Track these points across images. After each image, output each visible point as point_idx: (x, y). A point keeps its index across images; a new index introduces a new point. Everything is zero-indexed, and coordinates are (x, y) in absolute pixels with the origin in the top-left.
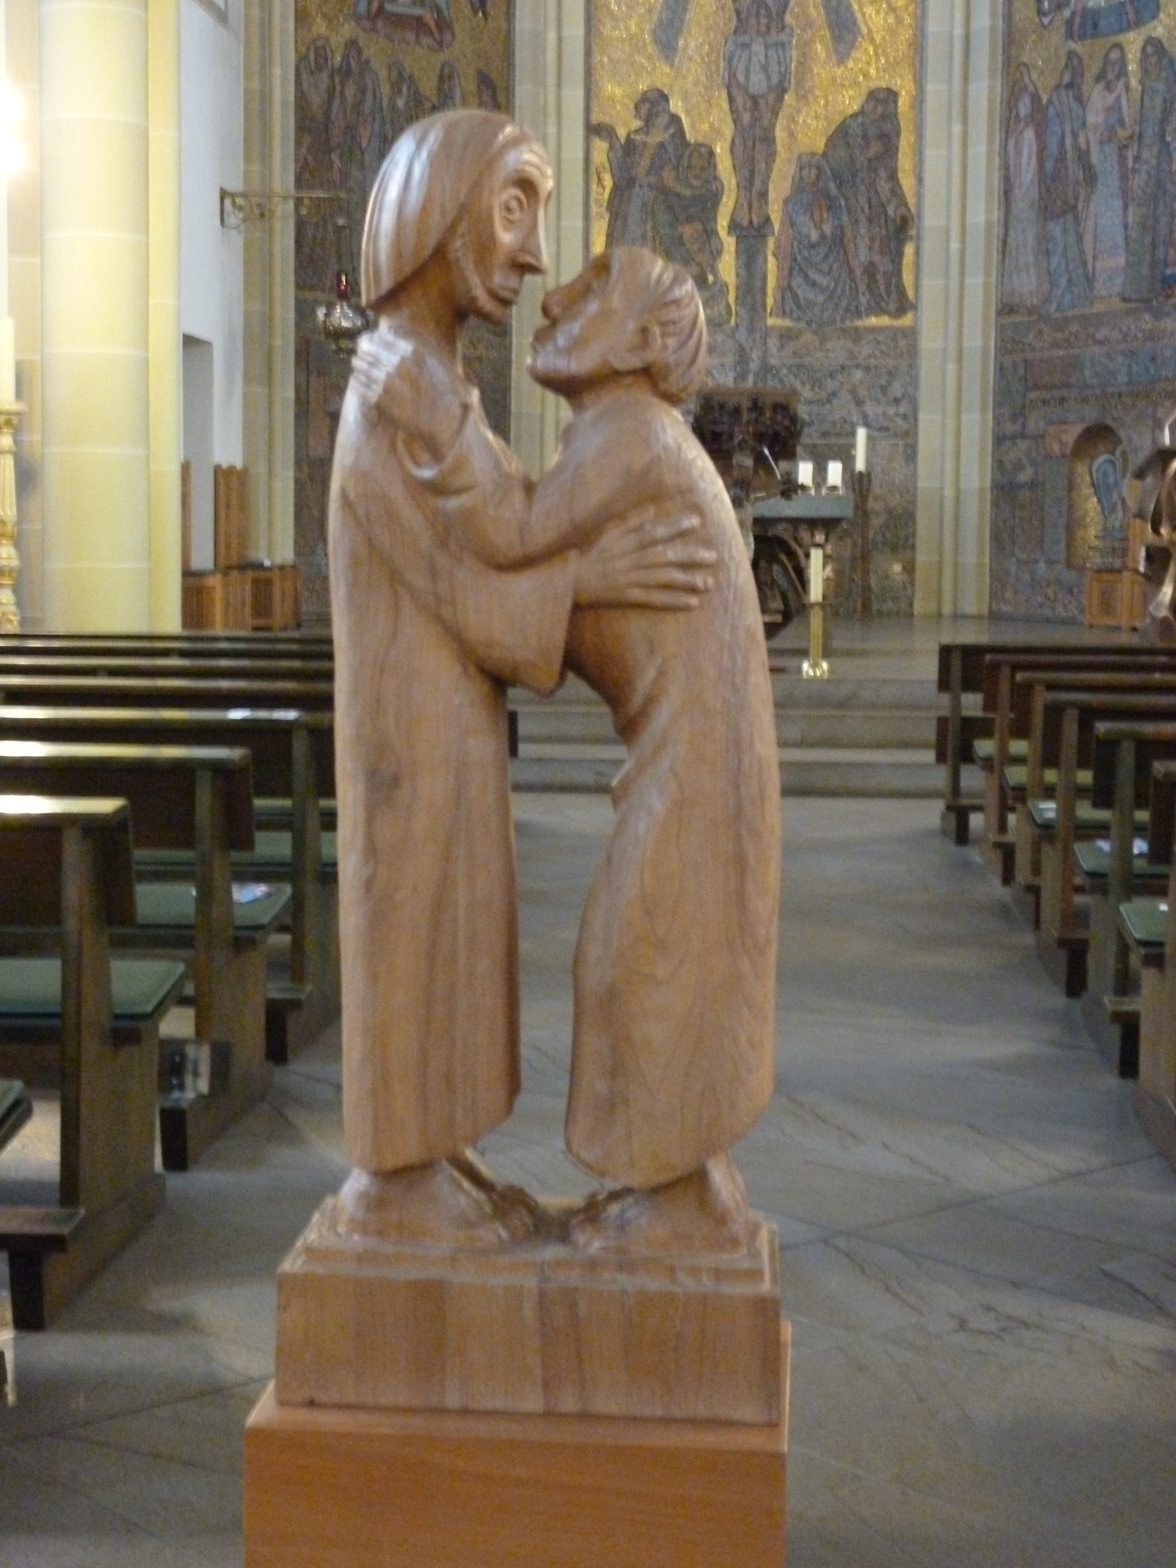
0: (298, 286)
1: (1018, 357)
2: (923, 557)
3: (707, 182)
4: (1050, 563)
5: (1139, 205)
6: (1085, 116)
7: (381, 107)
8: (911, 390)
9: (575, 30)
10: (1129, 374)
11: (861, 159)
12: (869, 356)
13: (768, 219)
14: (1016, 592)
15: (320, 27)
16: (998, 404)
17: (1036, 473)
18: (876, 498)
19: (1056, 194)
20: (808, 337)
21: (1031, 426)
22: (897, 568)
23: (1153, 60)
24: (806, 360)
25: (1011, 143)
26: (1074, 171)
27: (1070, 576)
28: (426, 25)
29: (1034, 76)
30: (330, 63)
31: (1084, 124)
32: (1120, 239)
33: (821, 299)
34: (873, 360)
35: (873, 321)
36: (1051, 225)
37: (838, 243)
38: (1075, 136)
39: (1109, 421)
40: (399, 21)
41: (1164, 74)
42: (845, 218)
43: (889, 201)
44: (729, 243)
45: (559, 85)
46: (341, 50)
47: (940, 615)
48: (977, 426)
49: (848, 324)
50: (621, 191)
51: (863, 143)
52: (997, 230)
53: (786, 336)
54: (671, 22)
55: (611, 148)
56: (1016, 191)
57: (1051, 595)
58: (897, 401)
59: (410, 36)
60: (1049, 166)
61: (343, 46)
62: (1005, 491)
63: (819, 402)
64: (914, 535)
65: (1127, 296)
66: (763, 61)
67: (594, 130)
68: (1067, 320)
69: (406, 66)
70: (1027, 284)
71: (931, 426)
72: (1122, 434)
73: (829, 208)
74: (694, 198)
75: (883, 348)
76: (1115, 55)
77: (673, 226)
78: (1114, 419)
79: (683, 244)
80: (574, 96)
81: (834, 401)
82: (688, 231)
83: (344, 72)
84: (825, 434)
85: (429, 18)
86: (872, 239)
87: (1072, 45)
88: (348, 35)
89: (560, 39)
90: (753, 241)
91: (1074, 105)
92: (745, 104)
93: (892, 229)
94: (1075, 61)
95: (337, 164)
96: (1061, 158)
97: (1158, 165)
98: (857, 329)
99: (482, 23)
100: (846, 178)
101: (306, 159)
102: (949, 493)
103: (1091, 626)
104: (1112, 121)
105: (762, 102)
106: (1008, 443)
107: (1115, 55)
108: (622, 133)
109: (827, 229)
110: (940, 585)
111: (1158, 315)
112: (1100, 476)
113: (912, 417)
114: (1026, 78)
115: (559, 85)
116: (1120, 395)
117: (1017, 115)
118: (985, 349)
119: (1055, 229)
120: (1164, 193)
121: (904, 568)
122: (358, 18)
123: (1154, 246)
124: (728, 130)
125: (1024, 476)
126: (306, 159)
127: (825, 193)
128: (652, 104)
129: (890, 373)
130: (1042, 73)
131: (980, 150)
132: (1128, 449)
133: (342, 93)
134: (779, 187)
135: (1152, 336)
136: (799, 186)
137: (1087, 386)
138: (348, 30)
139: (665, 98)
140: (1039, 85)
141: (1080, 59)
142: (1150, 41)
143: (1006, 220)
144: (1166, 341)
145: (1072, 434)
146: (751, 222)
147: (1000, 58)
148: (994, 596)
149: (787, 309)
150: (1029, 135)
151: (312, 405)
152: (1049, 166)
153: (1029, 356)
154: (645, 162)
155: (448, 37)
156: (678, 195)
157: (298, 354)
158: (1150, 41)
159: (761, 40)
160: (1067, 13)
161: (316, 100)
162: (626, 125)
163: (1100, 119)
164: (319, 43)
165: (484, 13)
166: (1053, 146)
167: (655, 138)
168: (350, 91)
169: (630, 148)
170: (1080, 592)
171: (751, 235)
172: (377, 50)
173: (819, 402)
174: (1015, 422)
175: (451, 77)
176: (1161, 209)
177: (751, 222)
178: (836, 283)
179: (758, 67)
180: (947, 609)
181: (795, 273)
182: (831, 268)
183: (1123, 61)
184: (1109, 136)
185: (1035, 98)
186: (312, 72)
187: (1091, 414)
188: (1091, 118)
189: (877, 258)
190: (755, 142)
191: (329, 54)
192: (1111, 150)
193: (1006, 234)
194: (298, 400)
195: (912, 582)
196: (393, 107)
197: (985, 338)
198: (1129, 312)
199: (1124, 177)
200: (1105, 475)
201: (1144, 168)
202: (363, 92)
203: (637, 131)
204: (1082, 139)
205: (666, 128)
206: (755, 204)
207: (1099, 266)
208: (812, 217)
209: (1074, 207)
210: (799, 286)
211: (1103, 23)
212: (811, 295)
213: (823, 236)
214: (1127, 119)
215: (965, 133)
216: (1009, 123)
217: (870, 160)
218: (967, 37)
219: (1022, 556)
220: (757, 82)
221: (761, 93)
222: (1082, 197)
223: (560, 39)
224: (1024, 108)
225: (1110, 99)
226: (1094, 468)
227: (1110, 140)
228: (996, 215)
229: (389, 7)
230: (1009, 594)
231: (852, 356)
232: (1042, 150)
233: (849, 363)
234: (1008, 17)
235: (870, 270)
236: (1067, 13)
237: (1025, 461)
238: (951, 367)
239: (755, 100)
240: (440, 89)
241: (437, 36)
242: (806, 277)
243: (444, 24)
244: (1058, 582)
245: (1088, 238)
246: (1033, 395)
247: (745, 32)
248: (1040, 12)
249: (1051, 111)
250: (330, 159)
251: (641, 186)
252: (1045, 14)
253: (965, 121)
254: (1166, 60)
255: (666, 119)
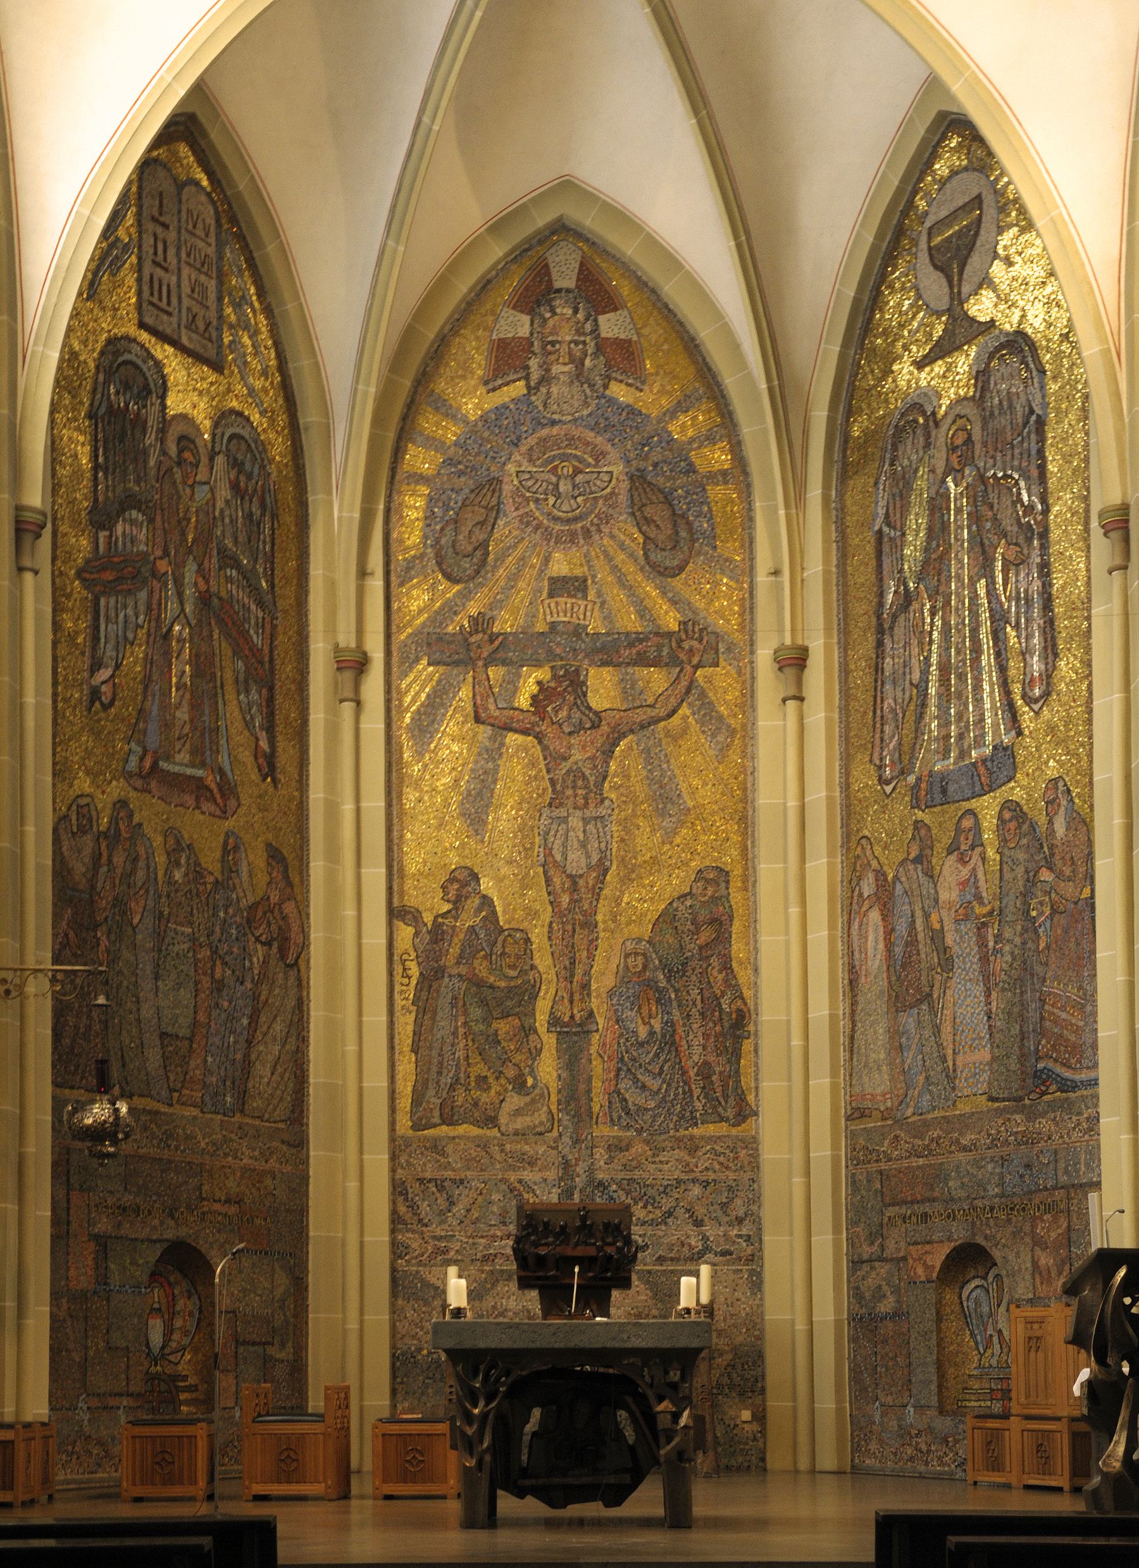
0: (56, 1084)
1: (874, 1167)
2: (776, 1403)
3: (523, 972)
4: (920, 1408)
5: (1003, 990)
6: (937, 892)
7: (156, 879)
8: (754, 1208)
9: (375, 802)
10: (1001, 1184)
11: (692, 948)
12: (707, 1169)
13: (591, 1014)
14: (881, 1441)
15: (83, 784)
16: (852, 1223)
17: (898, 1302)
18: (720, 1333)
19: (912, 983)
20: (638, 1148)
21: (891, 1245)
22: (746, 1415)
23: (1013, 825)
24: (637, 1174)
25: (856, 925)
26: (926, 953)
27: (943, 1424)
28: (208, 788)
29: (878, 850)
30: (95, 828)
31: (936, 901)
32: (984, 1033)
33: (652, 1104)
34: (710, 1173)
35: (711, 1129)
36: (903, 1017)
37: (669, 1042)
38: (927, 916)
39: (980, 1240)
40: (176, 782)
41: (1024, 841)
42: (676, 1015)
43: (723, 994)
44: (549, 1041)
45: (358, 864)
46: (108, 812)
47: (797, 1471)
48: (826, 1246)
49: (682, 1132)
50: (431, 977)
51: (692, 928)
52: (843, 1024)
53: (616, 1147)
54: (480, 793)
55: (416, 934)
56: (863, 980)
57: (924, 1448)
58: (740, 1221)
59: (190, 800)
60: (898, 950)
61: (110, 806)
62: (864, 1323)
63: (652, 1223)
64: (763, 1376)
65: (994, 1094)
66: (581, 837)
67: (396, 913)
68: (927, 1125)
69: (186, 836)
70: (878, 1084)
71: (780, 1251)
72: (997, 1254)
73: (658, 1001)
74: (510, 989)
75: (721, 1159)
76: (967, 823)
77: (487, 1020)
78: (986, 1237)
79: (499, 1042)
80: (375, 875)
81: (669, 1221)
82: (503, 1027)
83: (112, 837)
84: (661, 1260)
85: (211, 781)
86: (706, 1036)
87: (920, 815)
88: (115, 796)
89: (358, 810)
90: (575, 1038)
91: (923, 880)
92: (563, 884)
93: (726, 1025)
94: (923, 832)
95: (104, 942)
96: (912, 942)
97: (1024, 943)
98: (692, 1138)
99: (271, 789)
100: (676, 970)
101: (66, 935)
102: (801, 1326)
103: (975, 1483)
104: (969, 897)
105: (581, 882)
106: (866, 1267)
107: (967, 823)
108: (428, 918)
109: (657, 1025)
110: (795, 1431)
111: (1031, 1116)
112: (972, 1305)
113: (755, 1239)
114: (868, 853)
115: (358, 864)
116: (992, 1209)
117: (861, 895)
118: (835, 1160)
119: (908, 1020)
120: (1032, 975)
121: (753, 1415)
122: (128, 776)
123: (1023, 1036)
124: (547, 915)
125: (886, 1306)
126: (66, 935)
127: (651, 984)
128: (462, 884)
129: (730, 1189)
130: (886, 847)
131: (819, 936)
132: (1004, 1273)
133: (110, 861)
134: (604, 972)
135: (1027, 1140)
136: (625, 977)
137: (952, 1199)
138: (117, 789)
139: (475, 877)
140: (883, 860)
141: (929, 829)
142: (1009, 805)
143: (853, 1012)
144: (1042, 1143)
145: (938, 1256)
146: (572, 1017)
147: (839, 832)
148: (856, 1449)
149: (615, 1116)
150: (875, 916)
151: (74, 1226)
152: (898, 950)
153: (883, 1166)
154: (454, 951)
155: (233, 803)
156: (491, 987)
157: (55, 1164)
158: (1009, 805)
159: (578, 813)
160: (911, 779)
161: (79, 868)
162: (431, 903)
163: (954, 895)
164: (83, 801)
165: (274, 781)
166: (902, 928)
167: (468, 919)
168: (119, 859)
169: (438, 934)
170: (956, 1441)
171: (573, 1033)
172: (151, 813)
173: (652, 1223)
174: (872, 1243)
175: (236, 848)
176: (1028, 996)
177: (572, 1017)
178: (669, 1085)
179: (575, 843)
180: (804, 1464)
181: (623, 1074)
182: (661, 1068)
183: (977, 829)
184: (965, 914)
185: (880, 874)
186: (73, 834)
187: (960, 1234)
188: (944, 896)
189: (711, 1058)
190: (576, 923)
191: (94, 813)
192: (968, 927)
193: (853, 1030)
194: (55, 1222)
195: (763, 1432)
196: (170, 882)
197: (835, 1146)
198: (999, 1112)
199: (984, 959)
200: (977, 1303)
201: (1007, 948)
202: (136, 860)
203: (444, 915)
204: (934, 918)
205: (479, 910)
206: (577, 997)
207: (959, 1063)
208: (639, 1011)
209: (930, 995)
210: (627, 1090)
211: (952, 788)
212: (640, 1100)
213: (652, 1033)
214: (984, 894)
215: (804, 916)
216: (850, 907)
217: (701, 948)
218: (802, 808)
219: (889, 1400)
220: (576, 861)
221: (581, 872)
222: (937, 985)
223: (358, 810)
224: (868, 887)
225: (965, 872)
226: (964, 1297)
227: (966, 918)
228: (842, 1008)
229: (163, 765)
230: (873, 1446)
231: (688, 1168)
232: (889, 932)
233: (684, 1177)
234: (846, 787)
235: (705, 1072)
236: (911, 779)
237: (885, 1288)
238: (798, 1180)
239: (573, 879)
240: (223, 860)
241: (219, 801)
242: (636, 1080)
243: (227, 789)
244: (930, 1430)
245: (947, 1029)
246: (891, 1211)
247: (561, 804)
248: (882, 781)
249: (898, 886)
250: (95, 936)
251: (450, 976)
252: (888, 783)
253: (803, 903)
254: (1025, 827)
255: (477, 901)
